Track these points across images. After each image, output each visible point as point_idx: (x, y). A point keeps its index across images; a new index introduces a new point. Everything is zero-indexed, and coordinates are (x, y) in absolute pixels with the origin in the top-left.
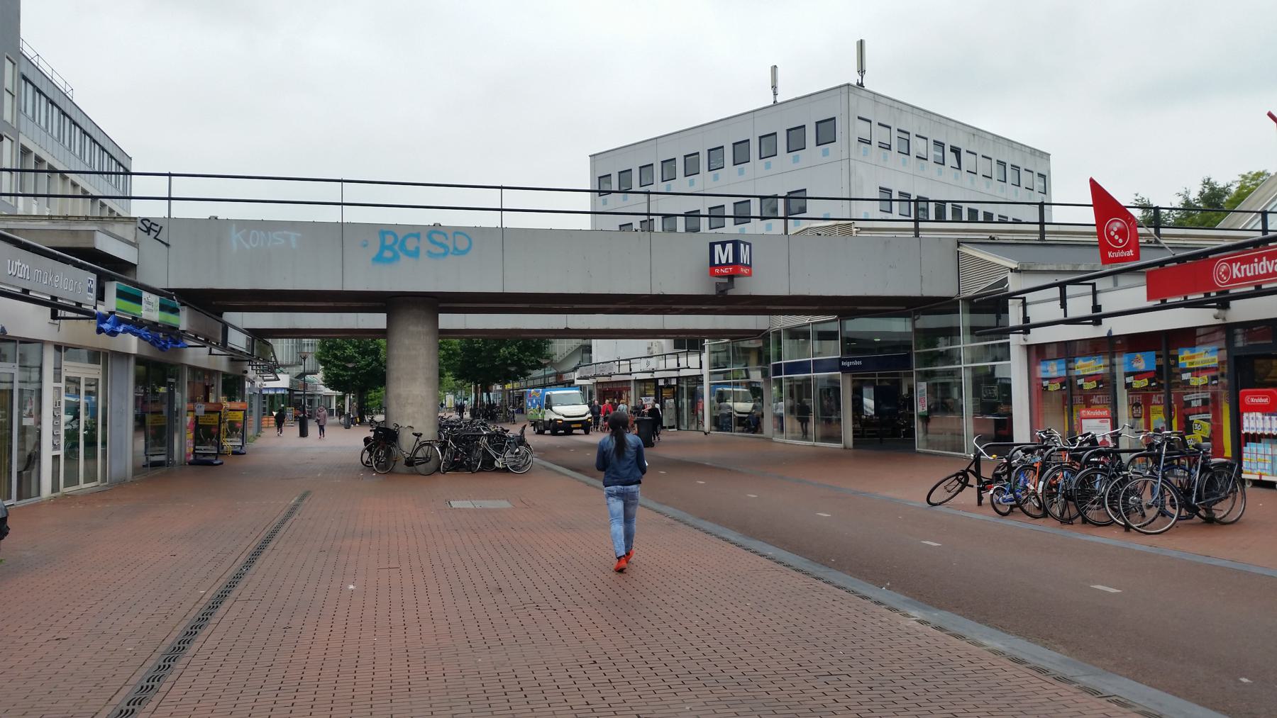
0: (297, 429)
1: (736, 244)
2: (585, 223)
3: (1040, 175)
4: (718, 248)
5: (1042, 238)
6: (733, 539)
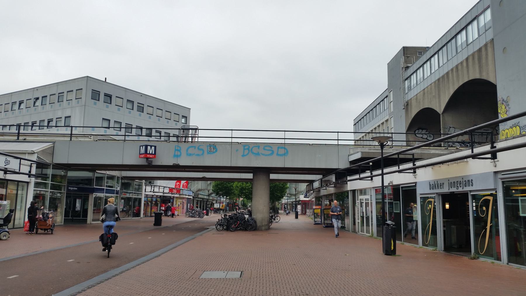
0: (294, 216)
1: (155, 147)
2: (352, 143)
3: (183, 117)
4: (149, 147)
5: (18, 139)
6: (117, 272)
